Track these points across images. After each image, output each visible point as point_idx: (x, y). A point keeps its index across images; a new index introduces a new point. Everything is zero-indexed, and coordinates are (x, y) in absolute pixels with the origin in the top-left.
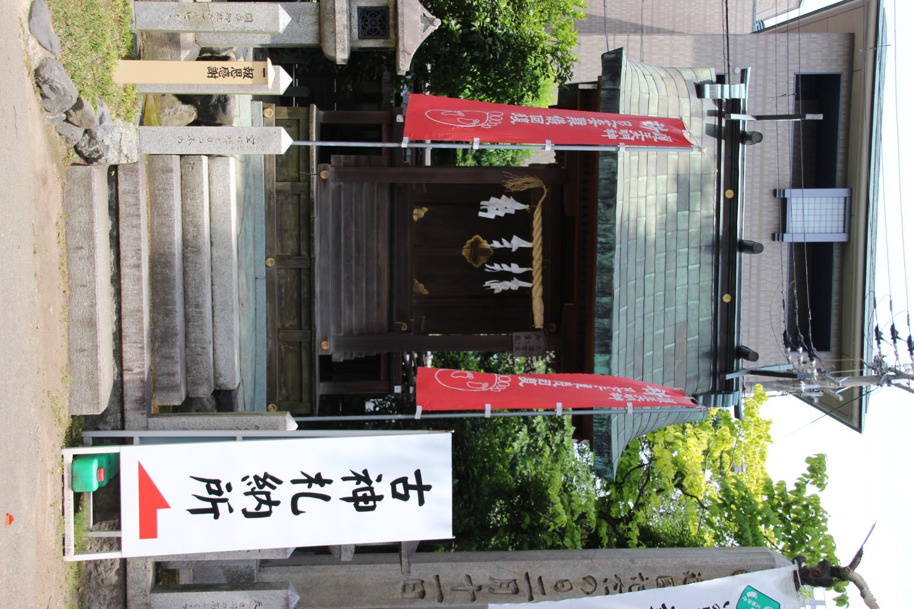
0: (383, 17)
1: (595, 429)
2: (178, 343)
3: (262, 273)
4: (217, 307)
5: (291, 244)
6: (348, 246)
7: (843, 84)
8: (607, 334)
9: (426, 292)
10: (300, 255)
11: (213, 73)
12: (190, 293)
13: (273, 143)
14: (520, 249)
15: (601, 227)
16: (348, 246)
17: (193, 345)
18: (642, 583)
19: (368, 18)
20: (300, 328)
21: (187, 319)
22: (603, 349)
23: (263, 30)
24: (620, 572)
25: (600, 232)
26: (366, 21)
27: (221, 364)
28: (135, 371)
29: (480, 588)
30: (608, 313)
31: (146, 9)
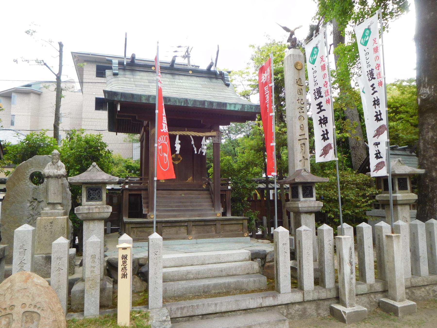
0: (91, 189)
1: (253, 111)
2: (242, 280)
3: (194, 241)
4: (218, 261)
5: (183, 230)
6: (179, 206)
7: (99, 64)
8: (219, 104)
9: (191, 178)
10: (187, 226)
11: (124, 276)
12: (218, 274)
13: (158, 242)
14: (179, 140)
15: (178, 104)
16: (179, 206)
17: (238, 272)
18: (300, 100)
19: (92, 196)
20: (216, 225)
21: (228, 276)
22: (225, 106)
23: (100, 249)
24: (297, 107)
25: (180, 105)
26: (93, 198)
27: (241, 258)
28: (262, 302)
29: (303, 157)
30: (211, 103)
31: (88, 310)
